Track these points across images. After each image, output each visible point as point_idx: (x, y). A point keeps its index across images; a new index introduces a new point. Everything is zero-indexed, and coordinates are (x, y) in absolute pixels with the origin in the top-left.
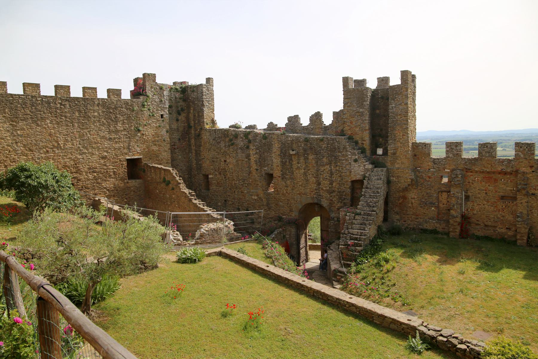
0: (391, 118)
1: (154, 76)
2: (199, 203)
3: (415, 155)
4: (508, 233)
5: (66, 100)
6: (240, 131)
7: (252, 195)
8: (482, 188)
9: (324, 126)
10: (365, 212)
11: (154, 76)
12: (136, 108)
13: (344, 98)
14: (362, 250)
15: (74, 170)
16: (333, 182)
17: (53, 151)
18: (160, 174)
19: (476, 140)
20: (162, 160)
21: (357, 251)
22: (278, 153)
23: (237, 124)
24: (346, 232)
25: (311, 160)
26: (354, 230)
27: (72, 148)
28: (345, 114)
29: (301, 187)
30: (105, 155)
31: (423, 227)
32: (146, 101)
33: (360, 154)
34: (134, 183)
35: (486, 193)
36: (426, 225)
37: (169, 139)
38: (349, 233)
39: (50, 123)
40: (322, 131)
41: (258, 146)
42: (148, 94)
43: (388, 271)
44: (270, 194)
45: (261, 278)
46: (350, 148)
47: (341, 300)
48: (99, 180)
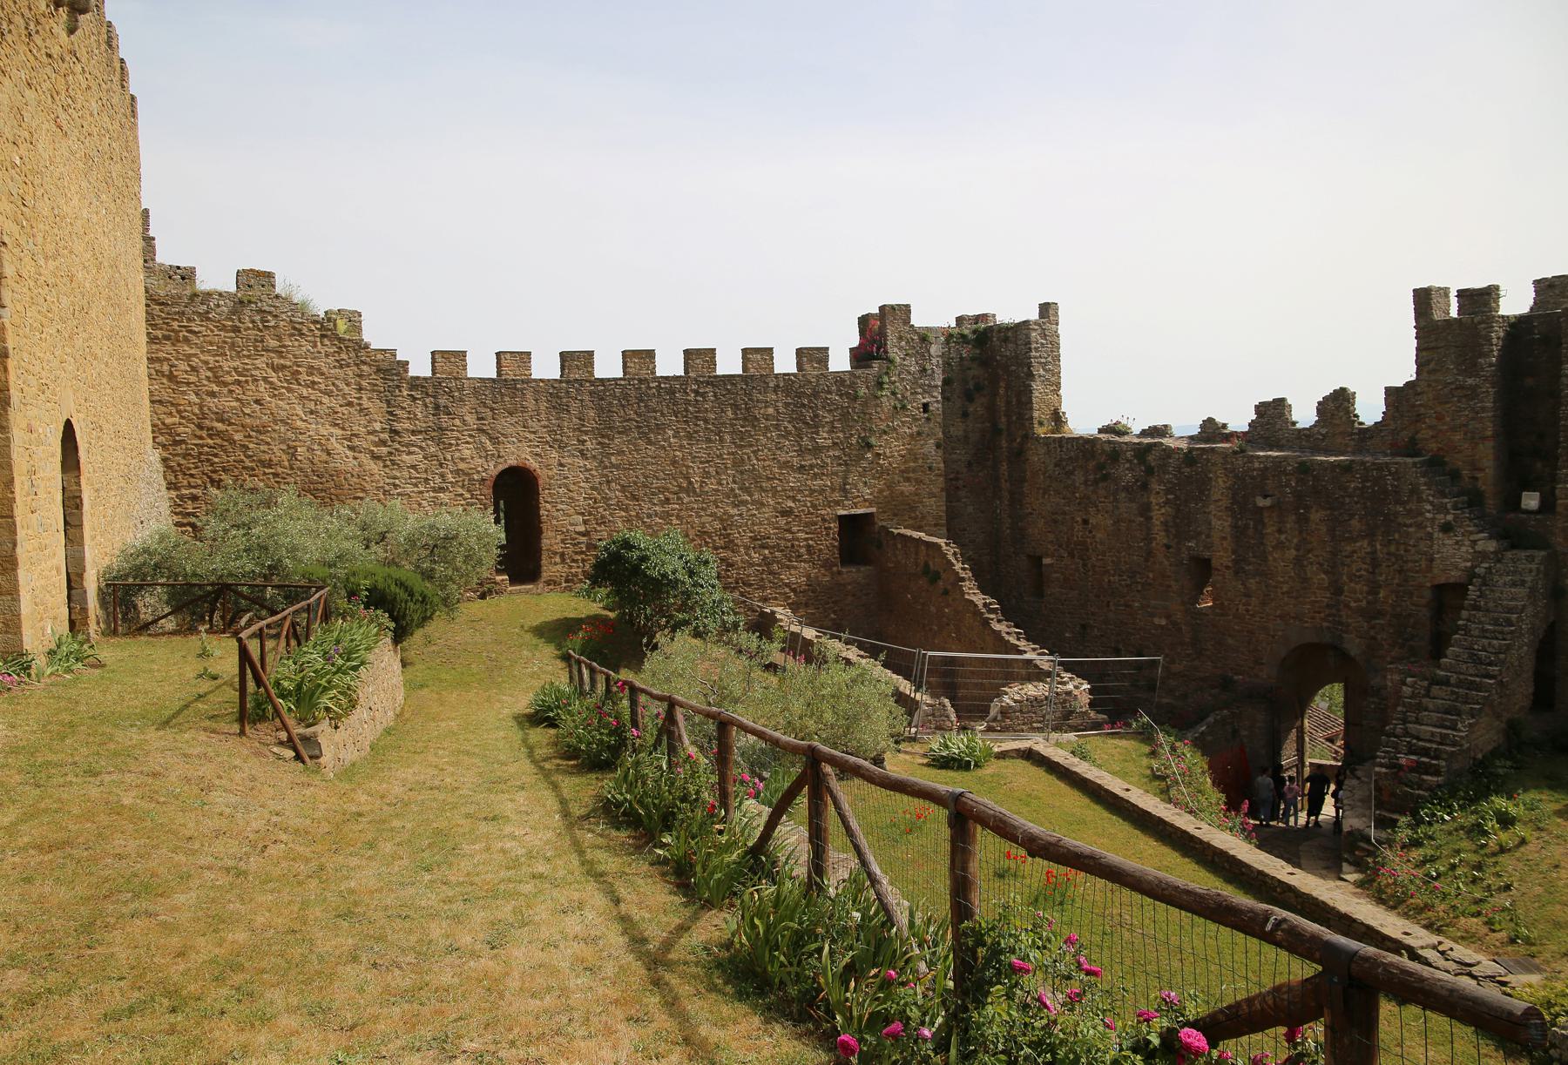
1: (906, 309)
2: (1008, 630)
5: (708, 383)
6: (1126, 443)
7: (1152, 615)
9: (1360, 429)
10: (1462, 677)
11: (906, 309)
12: (862, 391)
14: (1439, 786)
15: (719, 543)
17: (679, 498)
18: (917, 554)
20: (923, 517)
21: (1425, 785)
22: (1225, 503)
23: (1118, 423)
24: (1399, 730)
25: (1317, 524)
26: (1423, 727)
27: (718, 491)
28: (1419, 394)
29: (1286, 599)
30: (790, 507)
32: (887, 373)
33: (1461, 509)
34: (853, 575)
37: (942, 465)
38: (1407, 733)
39: (674, 437)
40: (1352, 443)
41: (1171, 482)
42: (891, 355)
43: (1503, 850)
44: (1202, 613)
45: (1106, 814)
46: (1432, 492)
47: (1267, 875)
48: (775, 567)
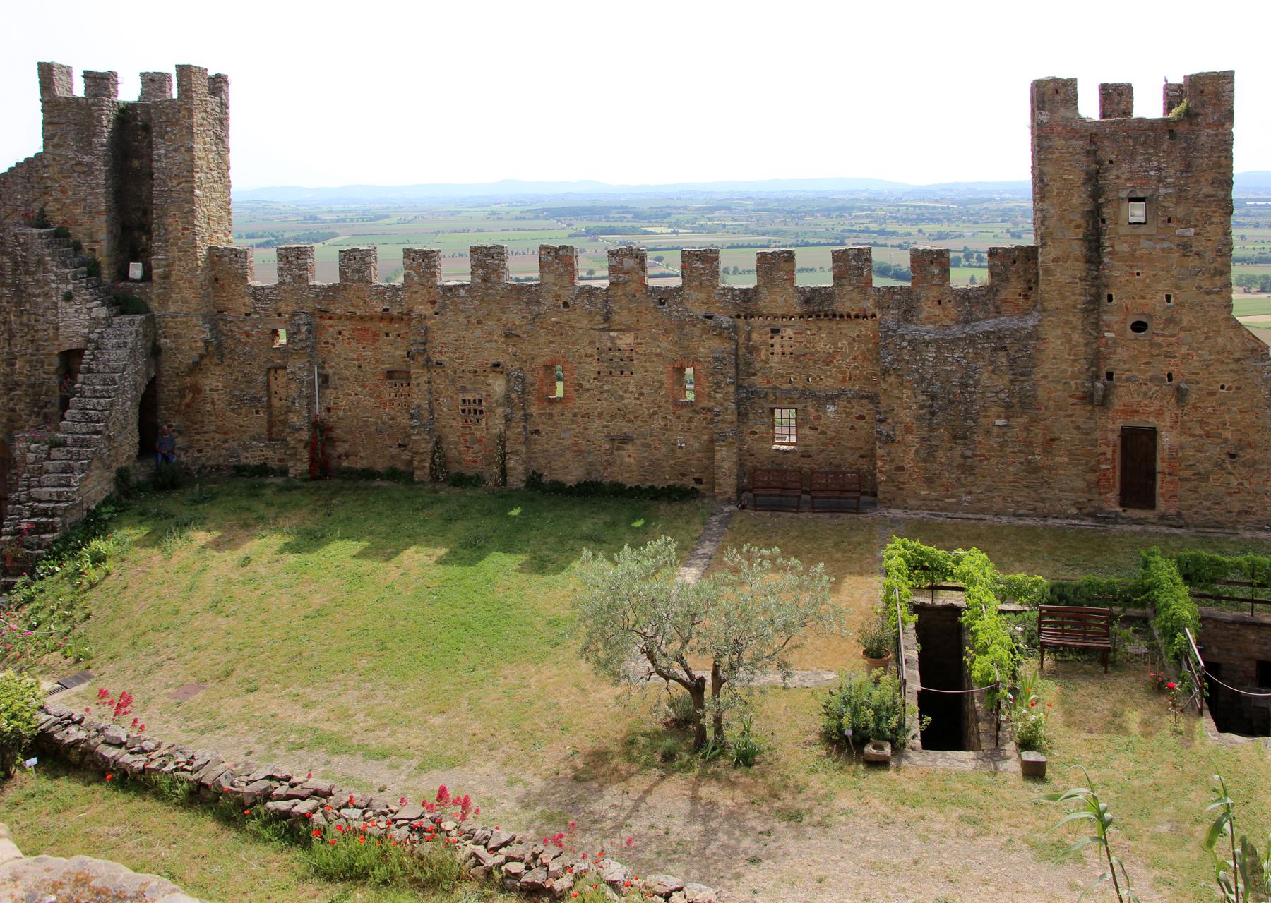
0: (159, 185)
3: (216, 280)
4: (403, 457)
8: (352, 354)
13: (45, 123)
16: (15, 358)
19: (615, 208)
24: (23, 497)
26: (44, 489)
31: (240, 461)
35: (360, 367)
36: (245, 454)
38: (30, 498)
